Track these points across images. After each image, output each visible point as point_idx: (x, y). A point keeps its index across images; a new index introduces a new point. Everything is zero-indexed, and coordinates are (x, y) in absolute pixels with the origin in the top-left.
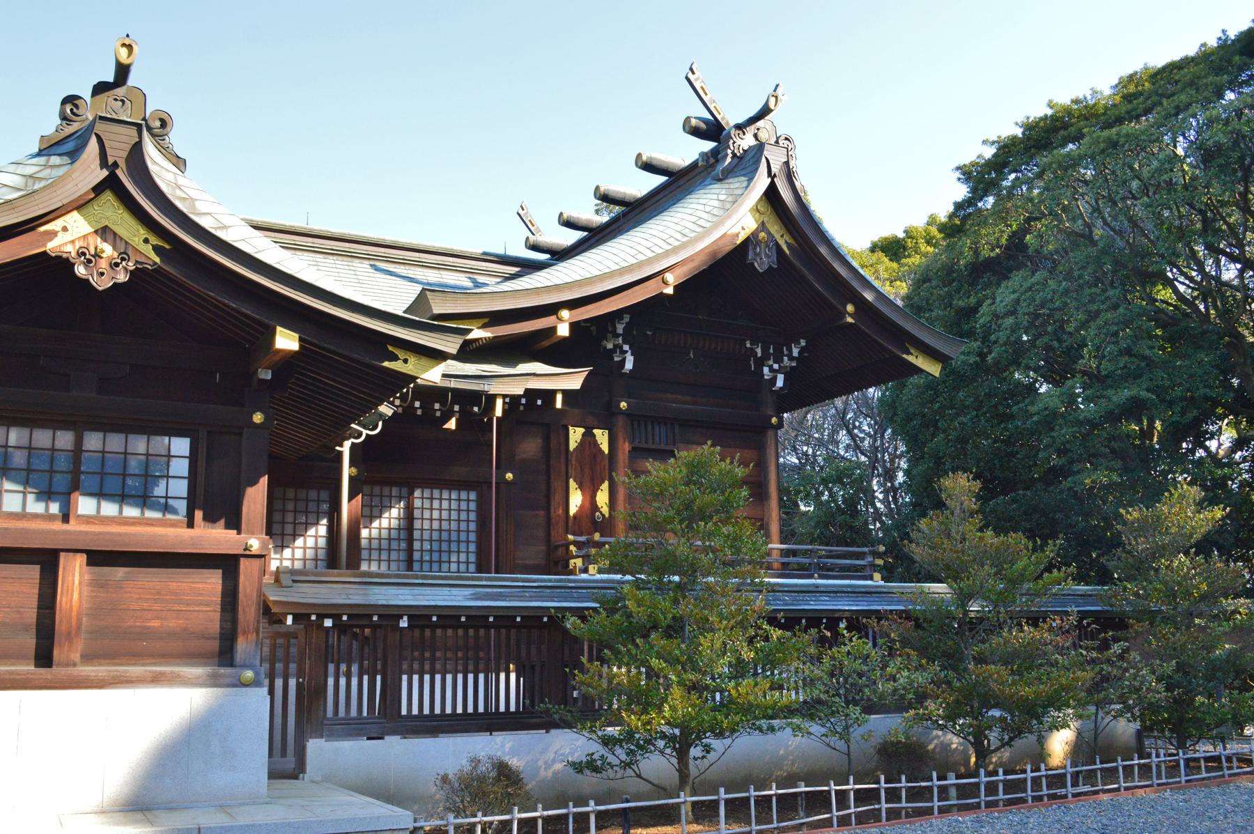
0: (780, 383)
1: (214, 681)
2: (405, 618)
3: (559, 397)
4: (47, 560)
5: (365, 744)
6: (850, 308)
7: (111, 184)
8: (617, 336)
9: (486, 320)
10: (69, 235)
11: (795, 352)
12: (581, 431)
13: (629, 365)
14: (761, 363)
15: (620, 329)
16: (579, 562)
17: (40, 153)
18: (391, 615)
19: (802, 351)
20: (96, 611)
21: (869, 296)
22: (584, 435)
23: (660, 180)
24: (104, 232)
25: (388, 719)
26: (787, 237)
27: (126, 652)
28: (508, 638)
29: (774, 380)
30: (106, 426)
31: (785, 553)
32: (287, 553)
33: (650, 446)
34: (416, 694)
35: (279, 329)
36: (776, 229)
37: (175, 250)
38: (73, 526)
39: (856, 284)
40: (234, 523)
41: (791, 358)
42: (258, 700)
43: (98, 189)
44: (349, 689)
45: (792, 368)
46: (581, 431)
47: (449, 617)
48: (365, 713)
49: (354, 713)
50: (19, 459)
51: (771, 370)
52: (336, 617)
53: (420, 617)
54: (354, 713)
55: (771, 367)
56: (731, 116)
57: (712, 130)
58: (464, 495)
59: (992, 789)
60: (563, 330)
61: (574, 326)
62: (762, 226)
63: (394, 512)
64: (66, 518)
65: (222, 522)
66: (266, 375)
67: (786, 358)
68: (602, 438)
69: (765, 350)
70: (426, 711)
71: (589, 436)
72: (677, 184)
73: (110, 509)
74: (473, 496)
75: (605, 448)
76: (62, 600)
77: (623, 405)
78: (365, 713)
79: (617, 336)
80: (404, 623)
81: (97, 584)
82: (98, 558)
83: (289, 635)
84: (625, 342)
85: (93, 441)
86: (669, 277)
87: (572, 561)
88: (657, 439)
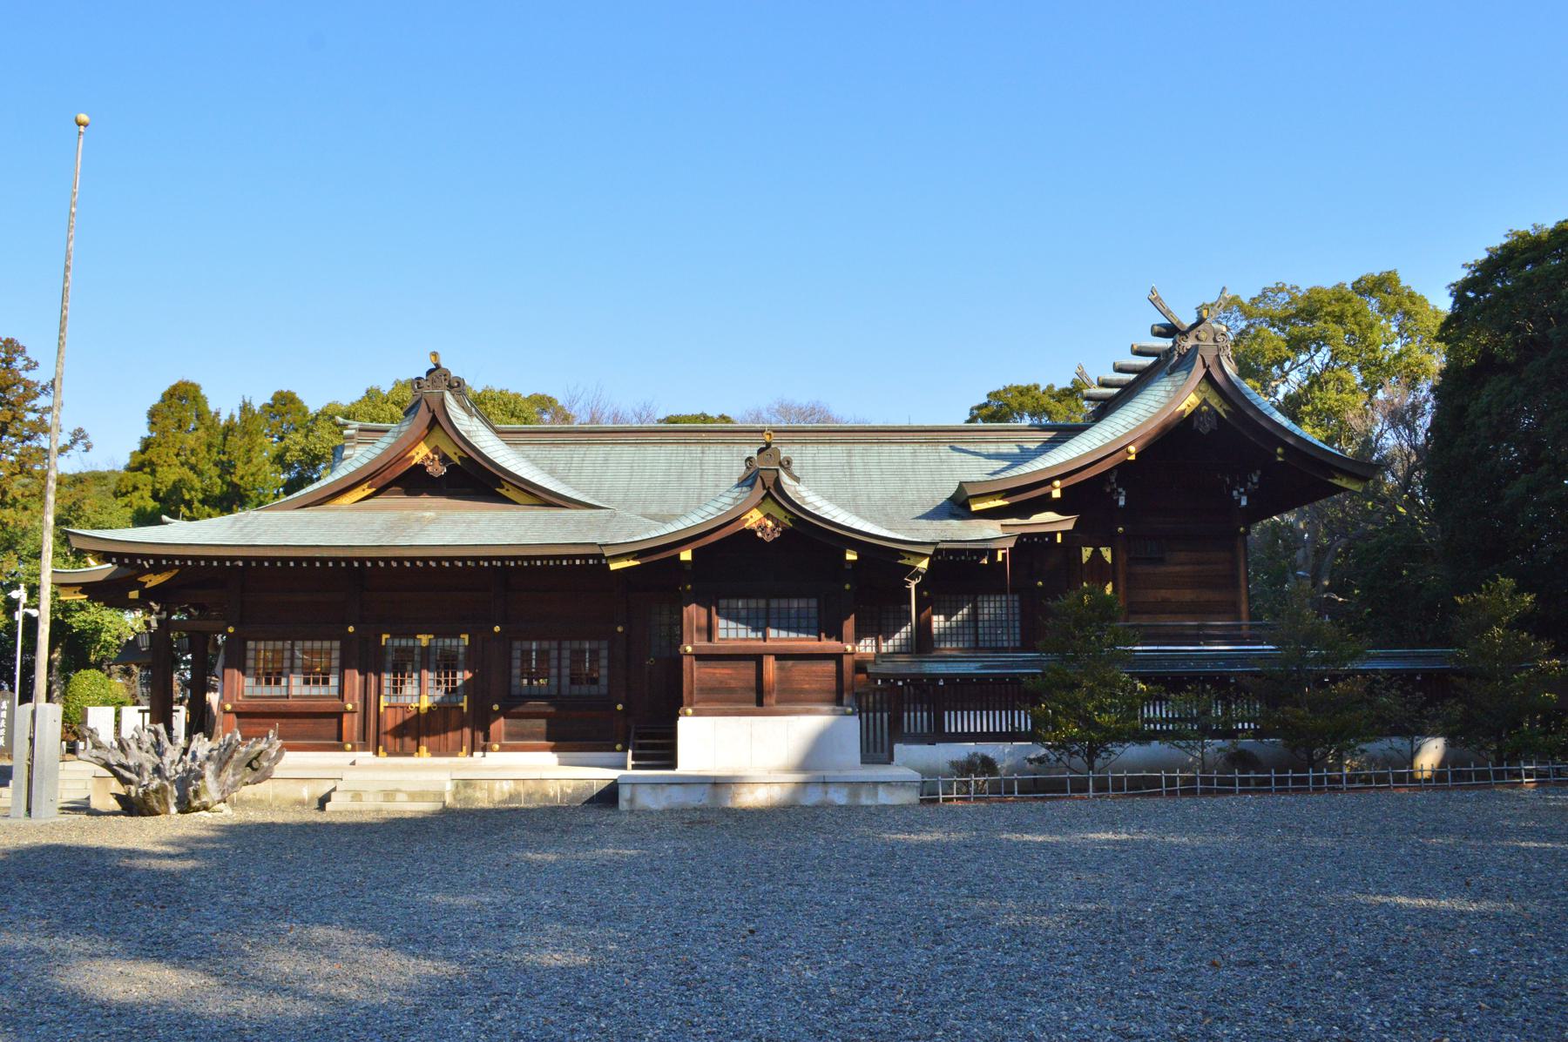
0: (1244, 503)
1: (834, 713)
4: (757, 658)
5: (927, 747)
6: (1279, 450)
7: (769, 494)
10: (754, 518)
11: (1255, 479)
17: (738, 486)
18: (934, 678)
19: (1260, 478)
20: (781, 681)
21: (1290, 441)
24: (768, 516)
25: (937, 735)
27: (791, 700)
28: (366, 684)
29: (1239, 501)
30: (779, 596)
31: (1251, 627)
32: (890, 642)
34: (955, 721)
36: (1215, 401)
37: (797, 521)
38: (768, 643)
39: (1278, 434)
40: (840, 638)
42: (853, 724)
43: (763, 499)
44: (916, 719)
47: (966, 678)
50: (743, 613)
52: (904, 680)
53: (949, 678)
56: (1187, 320)
57: (1170, 330)
59: (1319, 780)
60: (1056, 494)
61: (1063, 490)
62: (1205, 402)
63: (965, 611)
64: (765, 639)
65: (1385, 416)
68: (1107, 553)
72: (1144, 378)
73: (783, 634)
76: (766, 677)
81: (781, 669)
82: (781, 657)
83: (880, 689)
85: (774, 604)
86: (1132, 449)
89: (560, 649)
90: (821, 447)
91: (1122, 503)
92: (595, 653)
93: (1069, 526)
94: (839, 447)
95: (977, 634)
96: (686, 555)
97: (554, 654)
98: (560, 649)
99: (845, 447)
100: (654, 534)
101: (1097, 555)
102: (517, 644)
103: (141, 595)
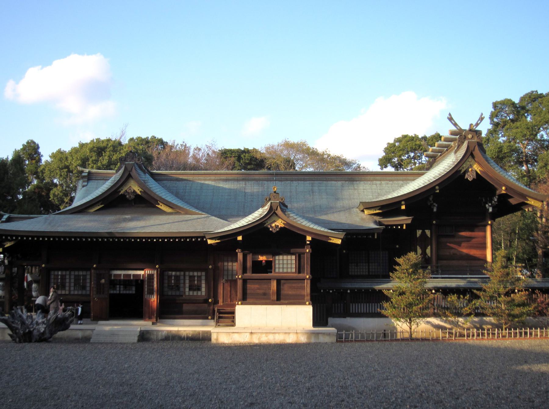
11: (496, 200)
12: (420, 231)
15: (431, 199)
26: (479, 168)
29: (488, 209)
34: (353, 308)
46: (420, 231)
52: (333, 290)
68: (428, 232)
75: (429, 235)
77: (434, 222)
89: (70, 275)
90: (299, 182)
91: (435, 210)
92: (199, 277)
93: (409, 222)
94: (308, 182)
95: (369, 269)
96: (240, 238)
97: (68, 277)
98: (70, 275)
99: (310, 182)
100: (226, 229)
101: (424, 233)
102: (52, 273)
103: (3, 250)
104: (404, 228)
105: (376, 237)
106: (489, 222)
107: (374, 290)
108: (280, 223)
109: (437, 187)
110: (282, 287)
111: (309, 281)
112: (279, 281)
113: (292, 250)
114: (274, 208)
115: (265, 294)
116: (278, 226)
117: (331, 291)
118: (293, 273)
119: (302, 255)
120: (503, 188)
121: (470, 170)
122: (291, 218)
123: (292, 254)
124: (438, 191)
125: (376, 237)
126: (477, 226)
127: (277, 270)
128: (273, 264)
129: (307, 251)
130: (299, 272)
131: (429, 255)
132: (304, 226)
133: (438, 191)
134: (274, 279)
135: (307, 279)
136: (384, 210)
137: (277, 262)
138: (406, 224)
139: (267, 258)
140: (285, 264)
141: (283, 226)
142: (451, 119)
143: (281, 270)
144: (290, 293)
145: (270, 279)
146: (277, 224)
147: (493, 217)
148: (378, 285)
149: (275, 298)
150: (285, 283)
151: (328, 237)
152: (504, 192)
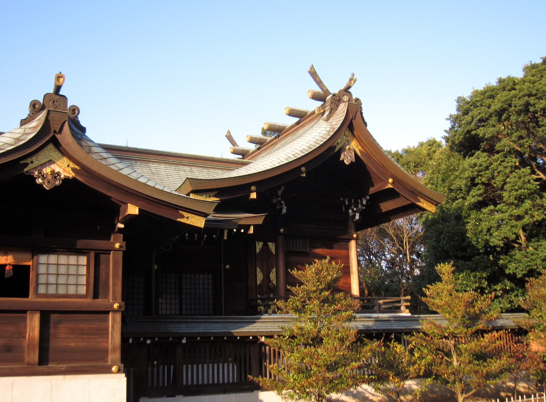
0: (357, 217)
2: (185, 339)
3: (252, 228)
8: (278, 197)
9: (217, 192)
11: (364, 202)
12: (261, 244)
13: (284, 211)
14: (348, 207)
15: (280, 193)
16: (262, 308)
22: (263, 245)
23: (296, 120)
26: (359, 147)
29: (354, 216)
33: (298, 250)
34: (191, 374)
35: (129, 205)
41: (362, 205)
45: (363, 210)
46: (261, 244)
48: (166, 385)
49: (161, 384)
51: (353, 211)
52: (152, 339)
54: (161, 384)
55: (353, 210)
58: (206, 276)
66: (121, 226)
67: (360, 205)
69: (350, 202)
70: (195, 383)
71: (265, 246)
74: (210, 276)
75: (273, 251)
77: (282, 230)
78: (166, 385)
79: (278, 197)
80: (184, 341)
84: (282, 199)
87: (259, 308)
88: (298, 246)
93: (260, 221)
101: (265, 247)
104: (251, 231)
105: (225, 238)
106: (355, 236)
107: (232, 338)
108: (63, 168)
109: (303, 169)
110: (52, 331)
111: (118, 317)
112: (46, 317)
113: (81, 243)
114: (55, 126)
115: (8, 349)
116: (59, 174)
117: (149, 342)
118: (81, 296)
119: (102, 257)
120: (390, 180)
121: (348, 147)
122: (94, 156)
123: (79, 252)
124: (304, 175)
125: (225, 238)
126: (337, 240)
127: (42, 290)
128: (32, 275)
129: (117, 245)
130: (96, 296)
131: (274, 282)
132: (126, 177)
133: (304, 175)
134: (34, 310)
135: (115, 311)
136: (224, 198)
137: (42, 269)
138: (255, 226)
139: (15, 259)
140: (62, 274)
141: (71, 175)
142: (313, 74)
143: (52, 290)
144: (73, 344)
145: (25, 312)
146: (57, 169)
147: (360, 226)
148: (238, 328)
149: (35, 357)
150: (59, 322)
151: (177, 208)
152: (390, 186)
